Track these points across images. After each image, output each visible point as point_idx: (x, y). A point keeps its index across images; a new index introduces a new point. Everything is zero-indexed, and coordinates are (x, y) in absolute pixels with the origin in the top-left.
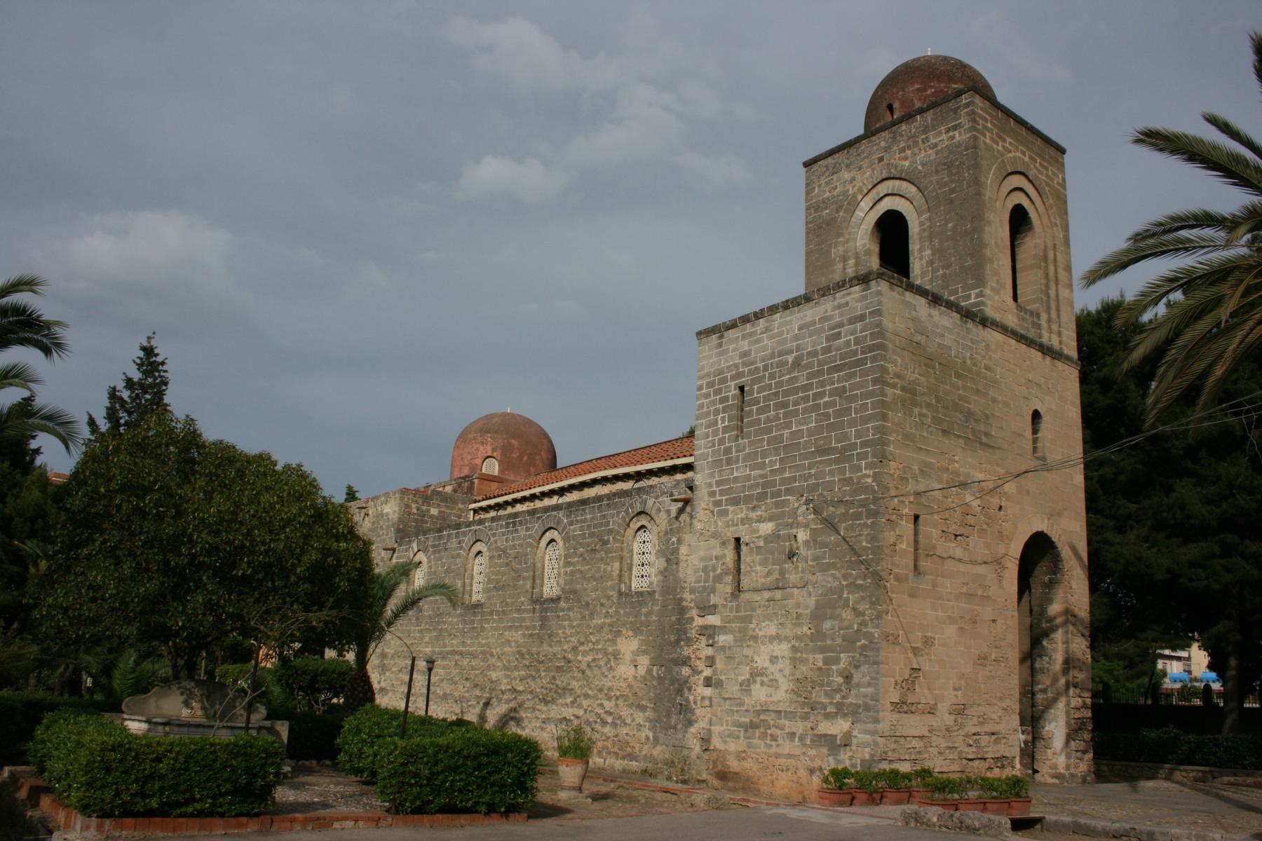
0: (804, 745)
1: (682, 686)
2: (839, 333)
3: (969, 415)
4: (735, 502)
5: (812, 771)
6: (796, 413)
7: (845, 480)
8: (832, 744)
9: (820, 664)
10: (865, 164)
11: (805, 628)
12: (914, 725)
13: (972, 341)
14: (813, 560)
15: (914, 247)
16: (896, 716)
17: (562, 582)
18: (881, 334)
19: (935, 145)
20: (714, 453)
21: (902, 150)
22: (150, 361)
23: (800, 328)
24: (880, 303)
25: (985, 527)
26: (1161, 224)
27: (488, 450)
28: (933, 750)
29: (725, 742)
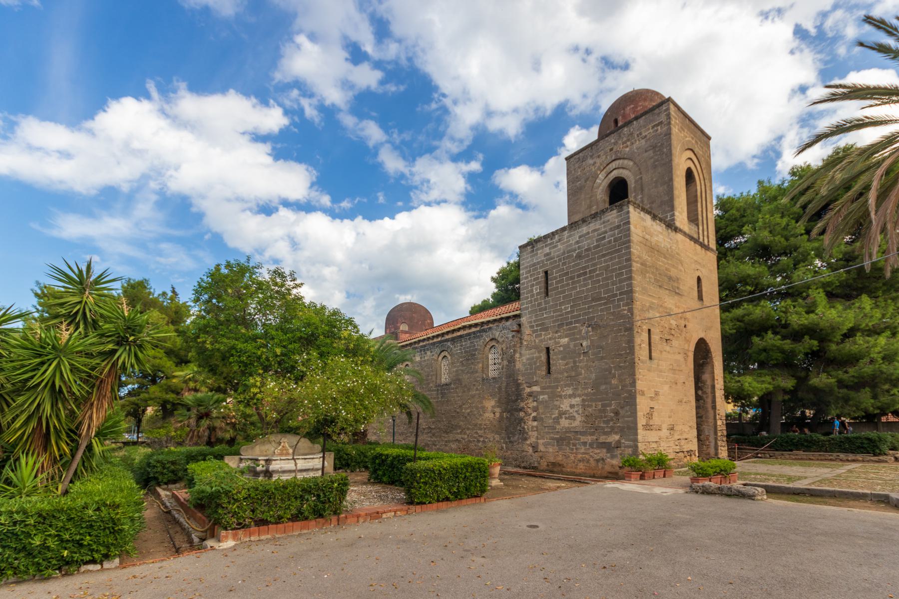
3: (670, 278)
6: (579, 282)
10: (602, 153)
19: (646, 136)
23: (580, 237)
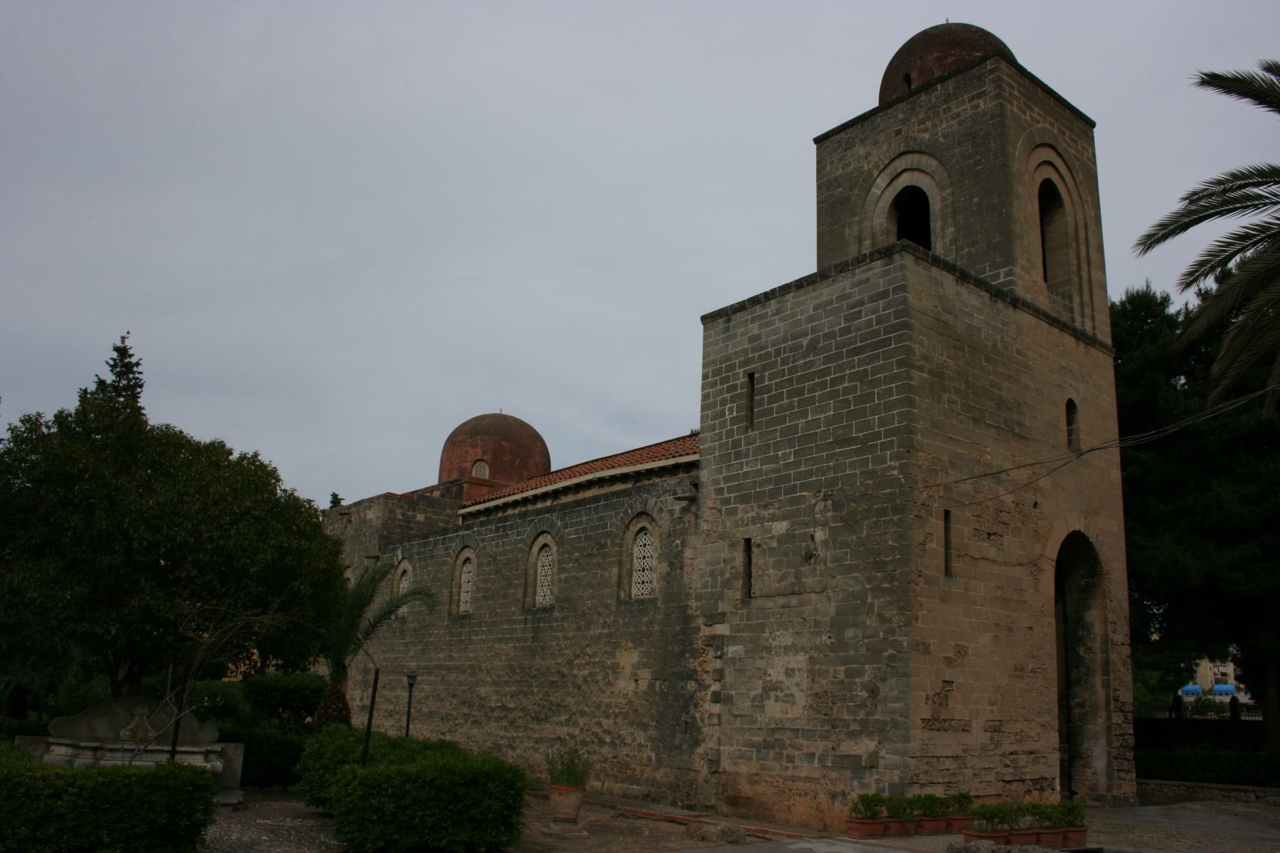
0: (825, 767)
1: (689, 702)
2: (860, 312)
4: (745, 499)
5: (833, 796)
6: (811, 401)
7: (868, 472)
8: (859, 767)
9: (842, 676)
11: (824, 638)
12: (946, 744)
13: (1003, 323)
14: (833, 562)
15: (936, 225)
16: (927, 734)
17: (556, 590)
18: (905, 310)
19: (958, 115)
20: (721, 446)
21: (921, 122)
22: (123, 361)
23: (816, 309)
24: (904, 278)
25: (1019, 525)
26: (1219, 182)
27: (478, 453)
28: (969, 772)
29: (736, 764)
